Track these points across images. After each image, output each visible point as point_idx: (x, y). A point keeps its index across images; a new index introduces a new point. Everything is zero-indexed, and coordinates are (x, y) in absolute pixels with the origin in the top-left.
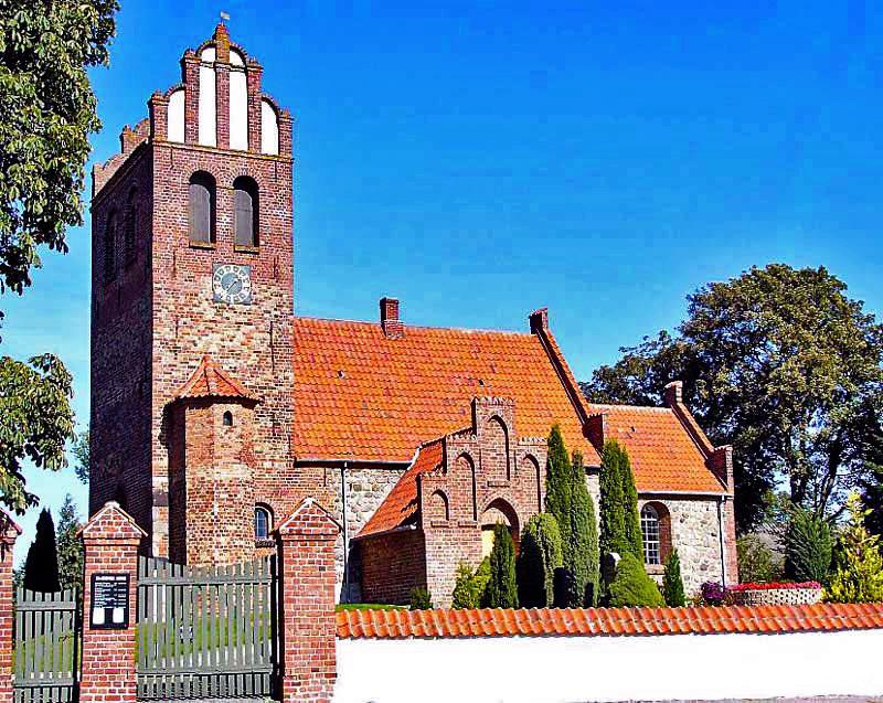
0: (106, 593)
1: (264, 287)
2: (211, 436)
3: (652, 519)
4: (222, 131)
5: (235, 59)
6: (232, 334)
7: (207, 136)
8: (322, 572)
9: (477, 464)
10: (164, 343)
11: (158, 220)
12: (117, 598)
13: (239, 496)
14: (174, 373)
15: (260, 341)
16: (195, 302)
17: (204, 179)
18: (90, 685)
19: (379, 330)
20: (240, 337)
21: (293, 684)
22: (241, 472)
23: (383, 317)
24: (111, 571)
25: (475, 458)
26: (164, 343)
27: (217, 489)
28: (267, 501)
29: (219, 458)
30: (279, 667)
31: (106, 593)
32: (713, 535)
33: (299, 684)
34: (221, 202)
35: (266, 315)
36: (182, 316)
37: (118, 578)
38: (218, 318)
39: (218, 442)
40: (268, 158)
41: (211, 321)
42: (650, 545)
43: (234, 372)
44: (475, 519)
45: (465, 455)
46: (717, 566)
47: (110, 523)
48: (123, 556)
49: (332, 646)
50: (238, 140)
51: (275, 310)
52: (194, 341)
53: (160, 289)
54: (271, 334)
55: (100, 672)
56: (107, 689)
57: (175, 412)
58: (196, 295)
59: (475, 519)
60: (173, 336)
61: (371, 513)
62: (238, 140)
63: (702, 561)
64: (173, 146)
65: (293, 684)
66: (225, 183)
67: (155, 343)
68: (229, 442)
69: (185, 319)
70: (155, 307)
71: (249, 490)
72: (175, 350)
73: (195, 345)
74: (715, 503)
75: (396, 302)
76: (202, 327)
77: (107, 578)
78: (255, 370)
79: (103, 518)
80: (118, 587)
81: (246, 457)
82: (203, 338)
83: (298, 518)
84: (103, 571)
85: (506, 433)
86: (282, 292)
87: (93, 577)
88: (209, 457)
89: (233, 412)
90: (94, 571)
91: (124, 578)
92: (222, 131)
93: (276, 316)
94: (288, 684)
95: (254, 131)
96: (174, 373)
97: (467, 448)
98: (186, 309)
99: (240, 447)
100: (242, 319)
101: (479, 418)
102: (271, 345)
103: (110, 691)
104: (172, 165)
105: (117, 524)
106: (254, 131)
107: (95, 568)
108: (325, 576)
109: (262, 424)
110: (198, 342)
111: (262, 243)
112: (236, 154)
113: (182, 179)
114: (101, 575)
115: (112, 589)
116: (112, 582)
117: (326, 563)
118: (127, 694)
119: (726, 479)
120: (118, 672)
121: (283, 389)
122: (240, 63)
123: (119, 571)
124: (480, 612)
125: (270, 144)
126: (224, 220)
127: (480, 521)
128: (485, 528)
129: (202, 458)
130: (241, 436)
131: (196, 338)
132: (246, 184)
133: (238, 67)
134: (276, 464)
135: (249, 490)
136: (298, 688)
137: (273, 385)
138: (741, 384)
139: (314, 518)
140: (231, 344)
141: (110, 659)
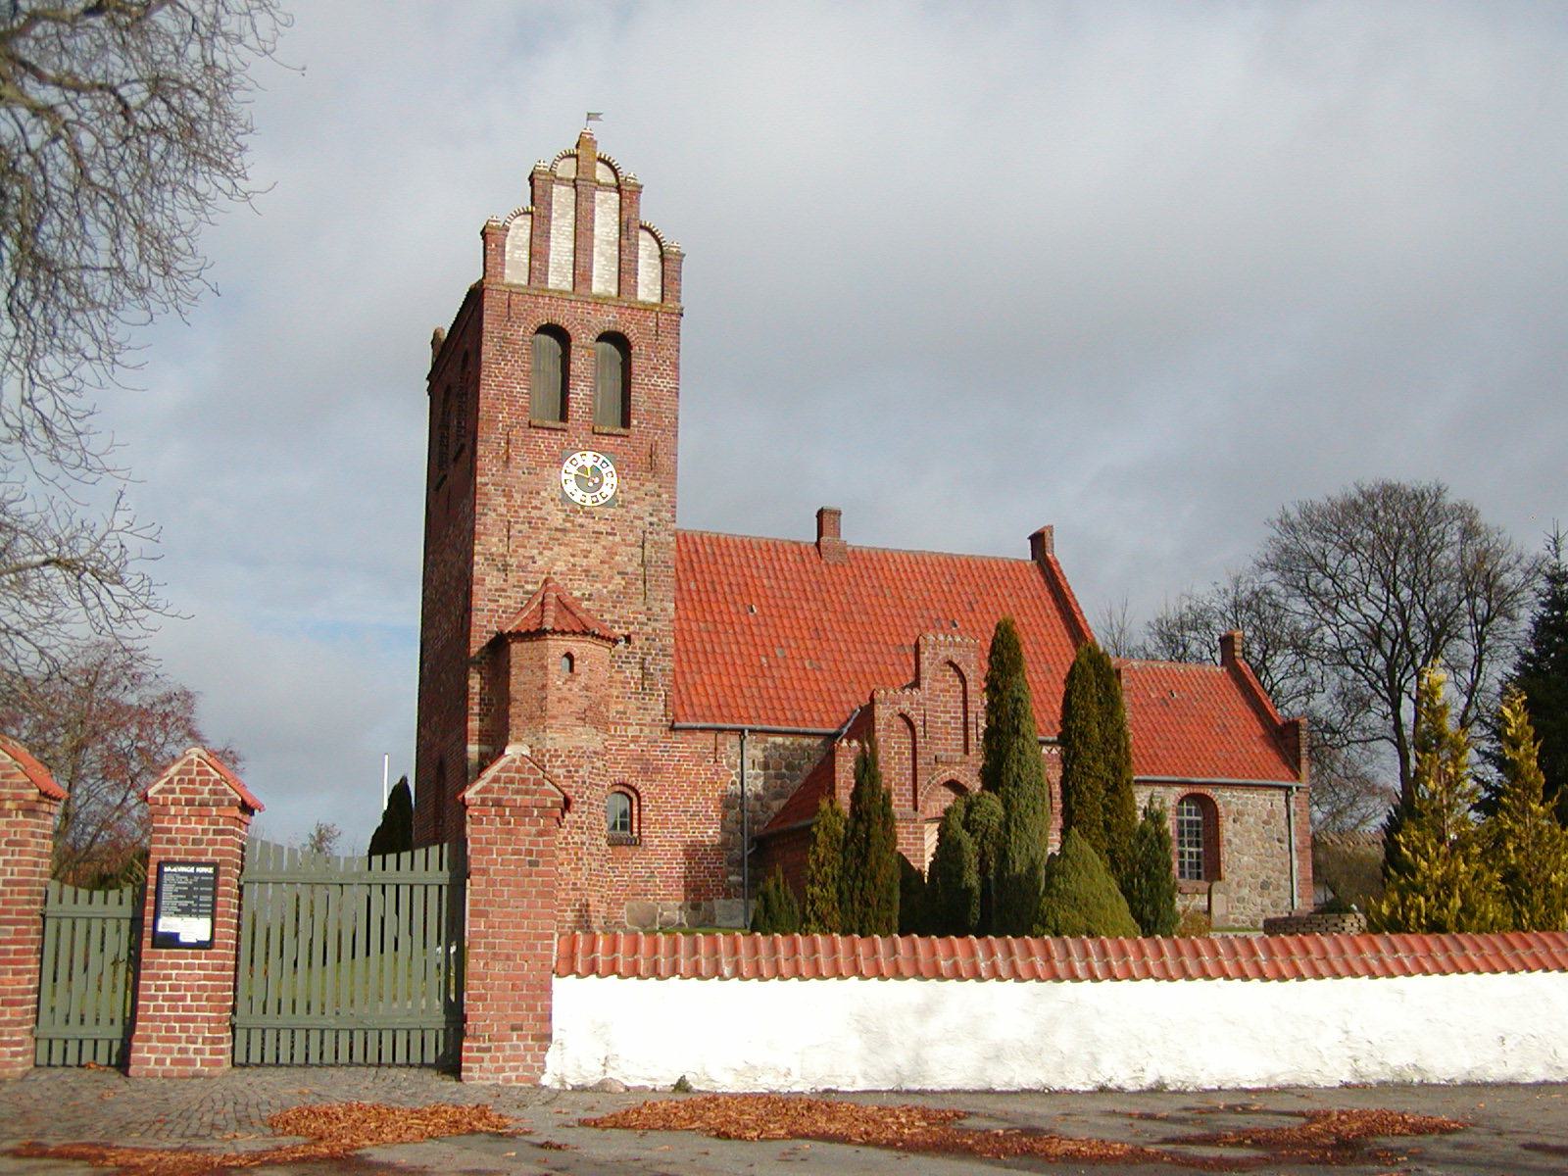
0: (180, 892)
1: (635, 484)
2: (544, 687)
3: (1194, 818)
4: (581, 273)
5: (603, 174)
6: (586, 546)
7: (559, 278)
8: (535, 869)
9: (920, 731)
10: (490, 559)
11: (488, 390)
12: (197, 901)
13: (581, 773)
14: (502, 601)
15: (627, 558)
16: (535, 503)
17: (558, 333)
18: (148, 1039)
19: (813, 552)
20: (598, 551)
21: (479, 1050)
22: (588, 738)
23: (820, 534)
24: (191, 858)
25: (918, 723)
26: (490, 559)
27: (550, 761)
28: (632, 781)
29: (554, 717)
30: (456, 1017)
31: (180, 892)
32: (1279, 840)
33: (488, 1050)
34: (577, 365)
35: (637, 523)
36: (516, 522)
37: (199, 870)
38: (568, 525)
39: (552, 696)
40: (647, 308)
41: (557, 529)
42: (1190, 854)
43: (589, 600)
44: (916, 809)
45: (904, 716)
46: (1283, 882)
47: (192, 781)
48: (211, 836)
49: (547, 989)
50: (603, 281)
51: (651, 515)
52: (533, 557)
53: (487, 484)
54: (643, 547)
55: (167, 1019)
56: (176, 1046)
57: (500, 644)
58: (538, 493)
59: (916, 809)
60: (503, 550)
61: (783, 802)
62: (603, 281)
63: (1263, 877)
64: (512, 290)
65: (479, 1050)
66: (583, 340)
67: (476, 558)
68: (569, 695)
69: (518, 527)
70: (478, 509)
71: (599, 764)
72: (505, 568)
73: (534, 562)
74: (1282, 792)
75: (838, 513)
76: (544, 537)
77: (183, 869)
78: (621, 597)
79: (179, 773)
80: (201, 883)
81: (593, 716)
82: (547, 553)
83: (496, 780)
84: (177, 858)
85: (965, 687)
86: (662, 490)
87: (160, 866)
88: (541, 717)
89: (576, 653)
90: (163, 858)
91: (210, 870)
92: (581, 273)
93: (651, 524)
94: (470, 1049)
95: (626, 271)
96: (502, 601)
97: (905, 706)
98: (523, 513)
99: (586, 703)
100: (602, 527)
101: (925, 664)
102: (643, 564)
103: (180, 1050)
104: (508, 315)
105: (202, 783)
106: (626, 271)
107: (166, 852)
108: (538, 874)
109: (628, 674)
110: (537, 558)
111: (634, 422)
112: (600, 301)
113: (522, 332)
114: (173, 863)
115: (190, 887)
116: (190, 876)
117: (540, 854)
118: (207, 1056)
119: (1298, 762)
120: (193, 1019)
121: (658, 625)
122: (612, 180)
123: (203, 859)
124: (901, 942)
125: (648, 289)
126: (580, 392)
127: (923, 812)
128: (927, 820)
129: (531, 718)
130: (587, 688)
131: (535, 552)
132: (618, 340)
133: (608, 185)
134: (646, 730)
135: (599, 764)
136: (487, 1056)
137: (642, 618)
138: (584, 782)
139: (523, 781)
140: (585, 562)
141: (183, 998)
